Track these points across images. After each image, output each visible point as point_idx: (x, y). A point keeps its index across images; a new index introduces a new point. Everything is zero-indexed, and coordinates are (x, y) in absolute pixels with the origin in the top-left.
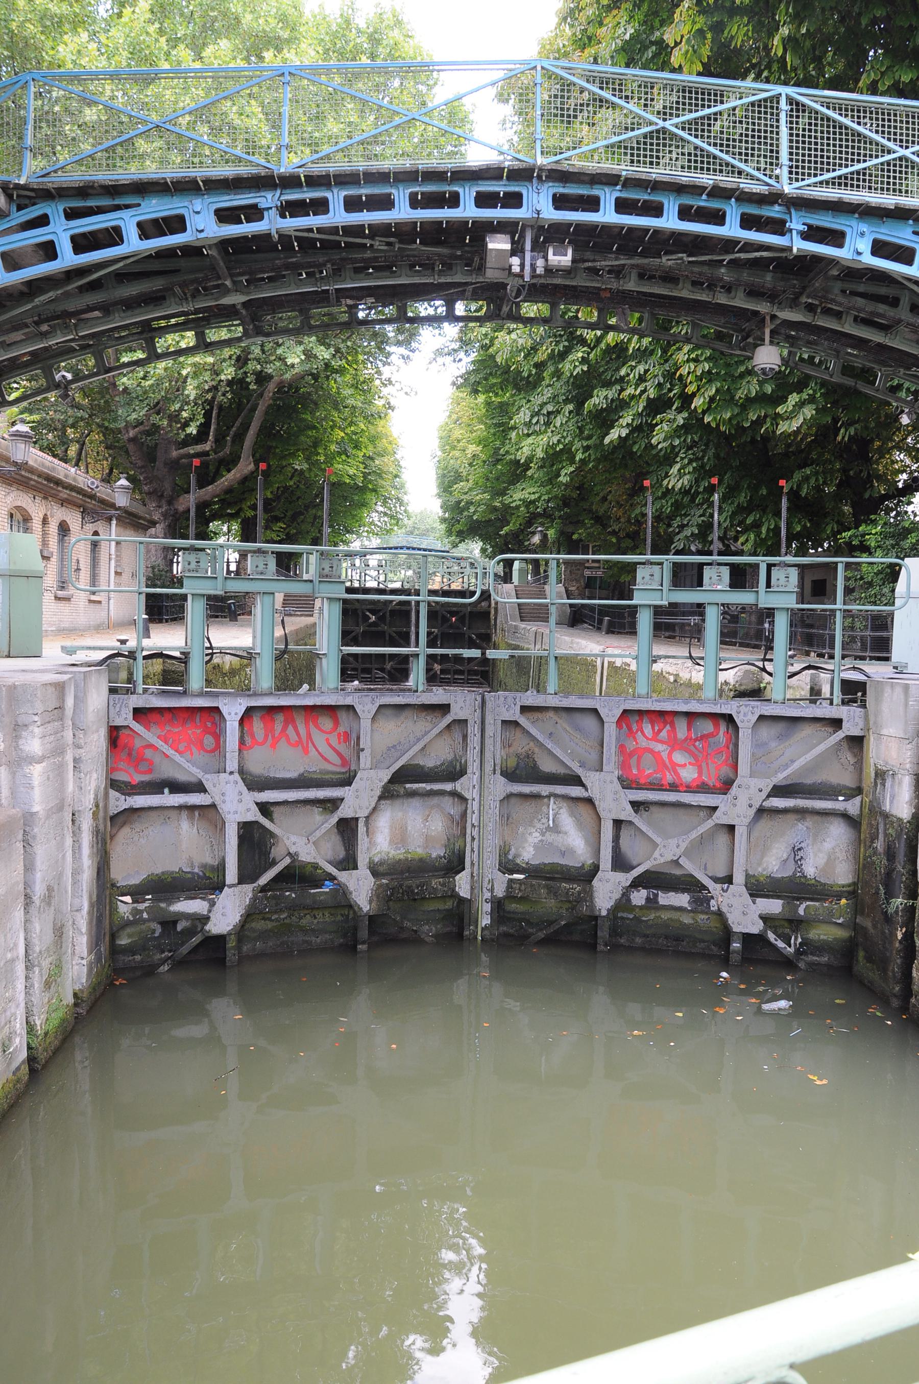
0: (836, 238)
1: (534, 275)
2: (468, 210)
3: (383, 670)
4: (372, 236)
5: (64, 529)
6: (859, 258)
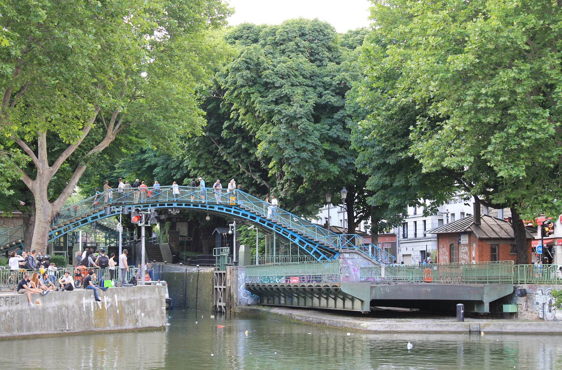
0: (213, 207)
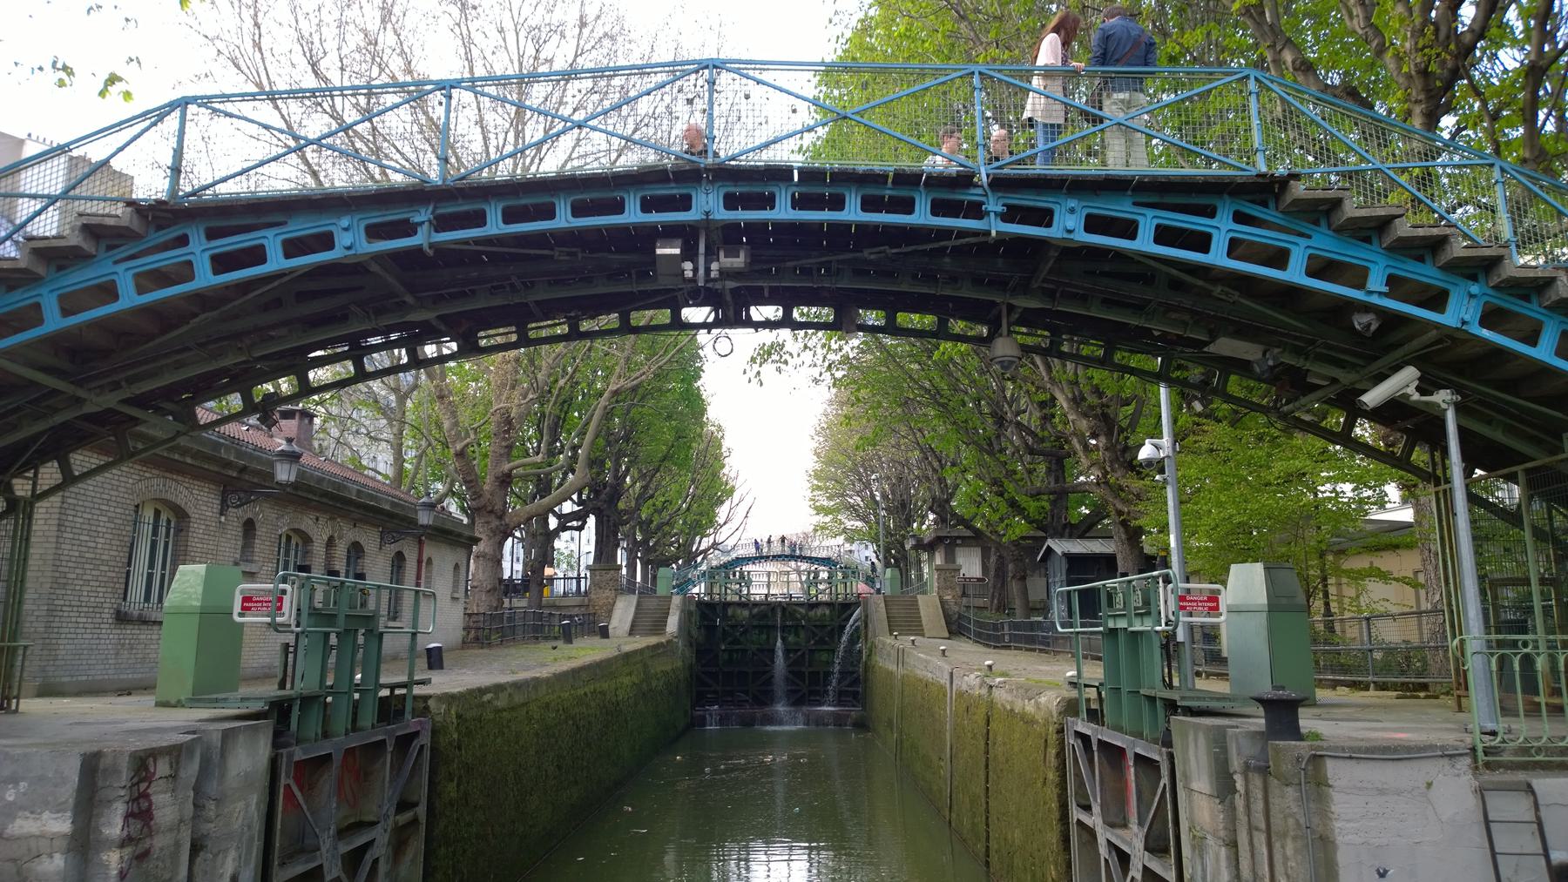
0: (1045, 217)
2: (634, 214)
3: (746, 693)
6: (1071, 236)
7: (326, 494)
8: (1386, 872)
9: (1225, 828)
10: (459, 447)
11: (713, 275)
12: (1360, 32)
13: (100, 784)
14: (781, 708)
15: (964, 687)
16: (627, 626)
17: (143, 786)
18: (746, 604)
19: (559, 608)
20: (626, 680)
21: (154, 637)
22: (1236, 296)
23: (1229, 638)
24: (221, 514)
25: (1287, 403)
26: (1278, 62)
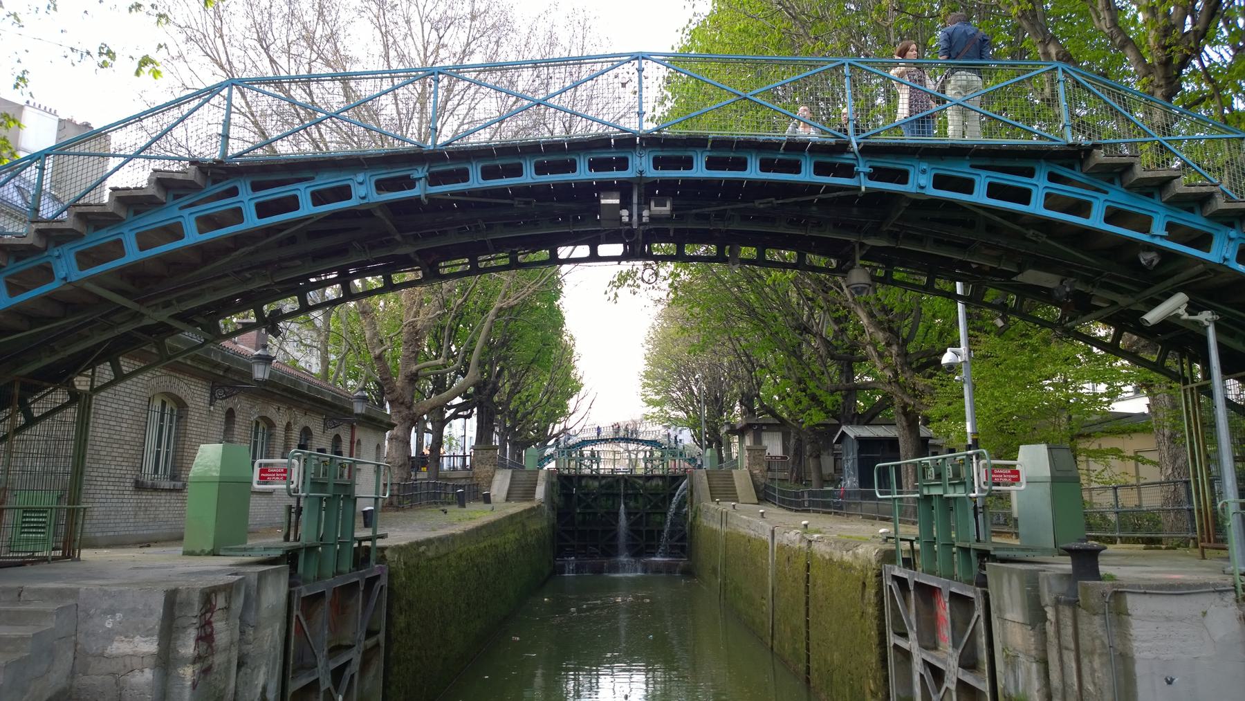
0: (902, 177)
1: (640, 223)
2: (583, 173)
3: (596, 546)
4: (511, 198)
5: (306, 432)
6: (923, 191)
7: (286, 389)
8: (1172, 680)
9: (1036, 649)
10: (377, 352)
11: (644, 220)
12: (1107, 31)
13: (177, 614)
14: (623, 559)
15: (785, 542)
16: (504, 494)
17: (208, 615)
18: (596, 477)
19: (450, 479)
20: (511, 536)
21: (162, 501)
22: (1043, 238)
23: (1019, 503)
24: (211, 405)
25: (1069, 321)
26: (1047, 54)
